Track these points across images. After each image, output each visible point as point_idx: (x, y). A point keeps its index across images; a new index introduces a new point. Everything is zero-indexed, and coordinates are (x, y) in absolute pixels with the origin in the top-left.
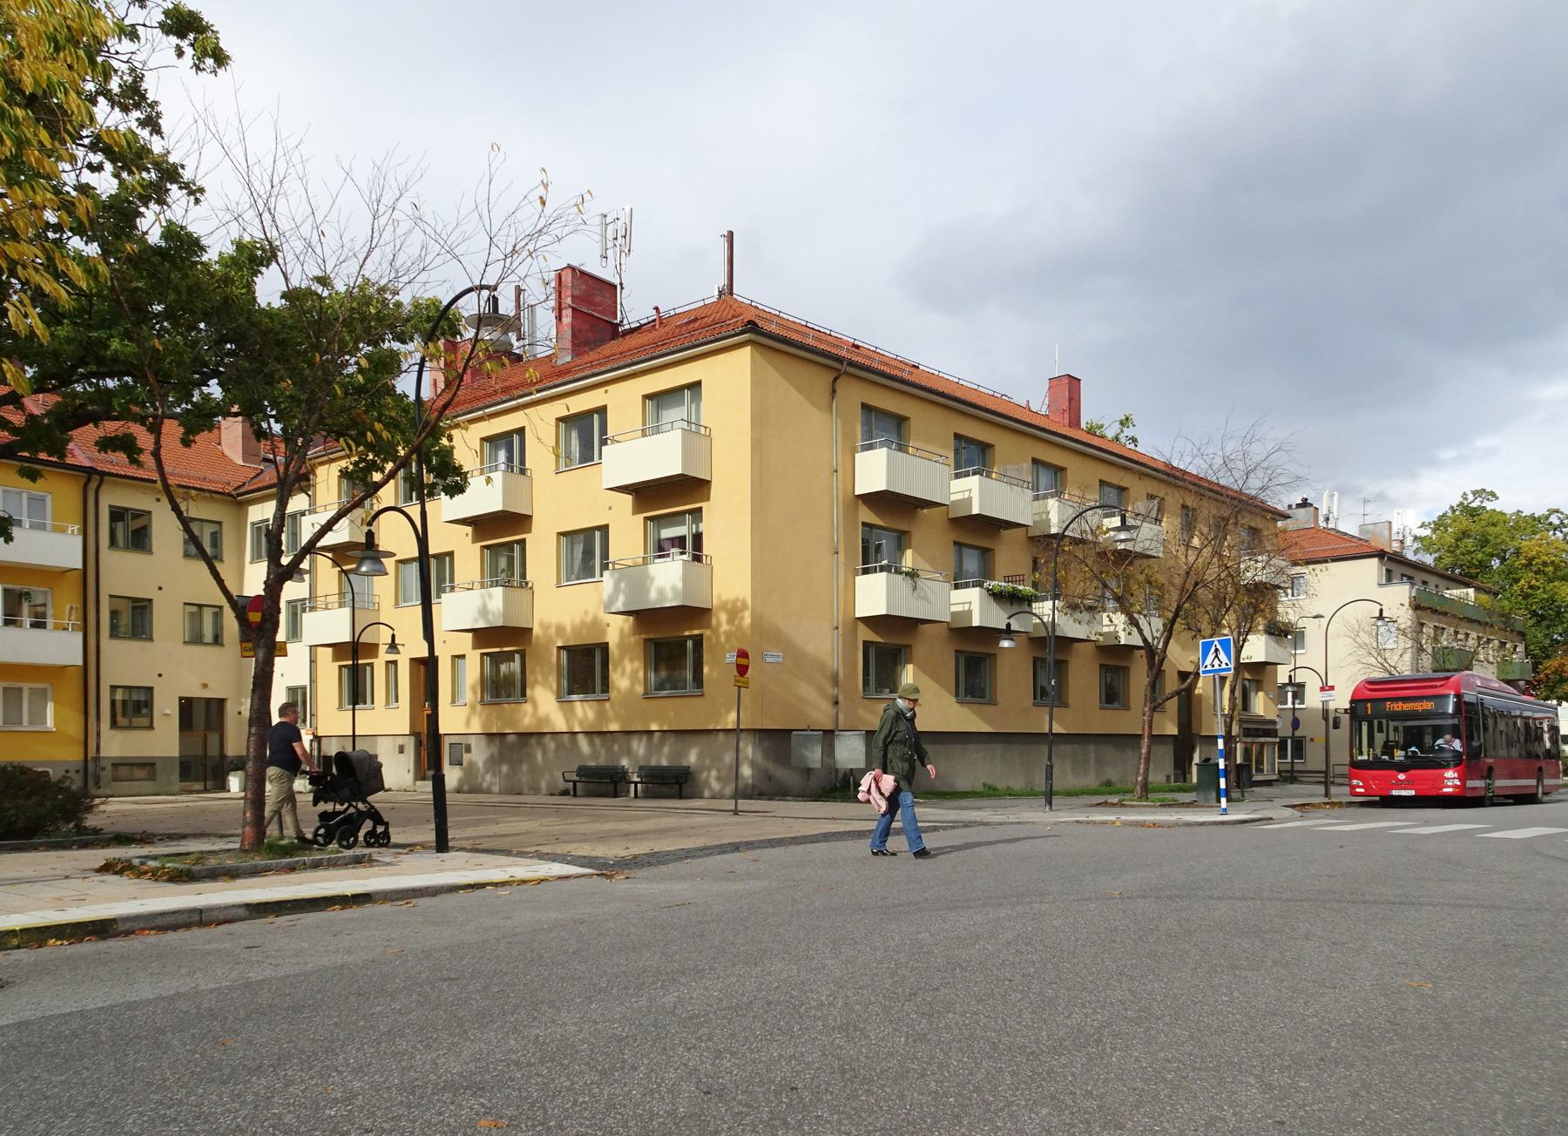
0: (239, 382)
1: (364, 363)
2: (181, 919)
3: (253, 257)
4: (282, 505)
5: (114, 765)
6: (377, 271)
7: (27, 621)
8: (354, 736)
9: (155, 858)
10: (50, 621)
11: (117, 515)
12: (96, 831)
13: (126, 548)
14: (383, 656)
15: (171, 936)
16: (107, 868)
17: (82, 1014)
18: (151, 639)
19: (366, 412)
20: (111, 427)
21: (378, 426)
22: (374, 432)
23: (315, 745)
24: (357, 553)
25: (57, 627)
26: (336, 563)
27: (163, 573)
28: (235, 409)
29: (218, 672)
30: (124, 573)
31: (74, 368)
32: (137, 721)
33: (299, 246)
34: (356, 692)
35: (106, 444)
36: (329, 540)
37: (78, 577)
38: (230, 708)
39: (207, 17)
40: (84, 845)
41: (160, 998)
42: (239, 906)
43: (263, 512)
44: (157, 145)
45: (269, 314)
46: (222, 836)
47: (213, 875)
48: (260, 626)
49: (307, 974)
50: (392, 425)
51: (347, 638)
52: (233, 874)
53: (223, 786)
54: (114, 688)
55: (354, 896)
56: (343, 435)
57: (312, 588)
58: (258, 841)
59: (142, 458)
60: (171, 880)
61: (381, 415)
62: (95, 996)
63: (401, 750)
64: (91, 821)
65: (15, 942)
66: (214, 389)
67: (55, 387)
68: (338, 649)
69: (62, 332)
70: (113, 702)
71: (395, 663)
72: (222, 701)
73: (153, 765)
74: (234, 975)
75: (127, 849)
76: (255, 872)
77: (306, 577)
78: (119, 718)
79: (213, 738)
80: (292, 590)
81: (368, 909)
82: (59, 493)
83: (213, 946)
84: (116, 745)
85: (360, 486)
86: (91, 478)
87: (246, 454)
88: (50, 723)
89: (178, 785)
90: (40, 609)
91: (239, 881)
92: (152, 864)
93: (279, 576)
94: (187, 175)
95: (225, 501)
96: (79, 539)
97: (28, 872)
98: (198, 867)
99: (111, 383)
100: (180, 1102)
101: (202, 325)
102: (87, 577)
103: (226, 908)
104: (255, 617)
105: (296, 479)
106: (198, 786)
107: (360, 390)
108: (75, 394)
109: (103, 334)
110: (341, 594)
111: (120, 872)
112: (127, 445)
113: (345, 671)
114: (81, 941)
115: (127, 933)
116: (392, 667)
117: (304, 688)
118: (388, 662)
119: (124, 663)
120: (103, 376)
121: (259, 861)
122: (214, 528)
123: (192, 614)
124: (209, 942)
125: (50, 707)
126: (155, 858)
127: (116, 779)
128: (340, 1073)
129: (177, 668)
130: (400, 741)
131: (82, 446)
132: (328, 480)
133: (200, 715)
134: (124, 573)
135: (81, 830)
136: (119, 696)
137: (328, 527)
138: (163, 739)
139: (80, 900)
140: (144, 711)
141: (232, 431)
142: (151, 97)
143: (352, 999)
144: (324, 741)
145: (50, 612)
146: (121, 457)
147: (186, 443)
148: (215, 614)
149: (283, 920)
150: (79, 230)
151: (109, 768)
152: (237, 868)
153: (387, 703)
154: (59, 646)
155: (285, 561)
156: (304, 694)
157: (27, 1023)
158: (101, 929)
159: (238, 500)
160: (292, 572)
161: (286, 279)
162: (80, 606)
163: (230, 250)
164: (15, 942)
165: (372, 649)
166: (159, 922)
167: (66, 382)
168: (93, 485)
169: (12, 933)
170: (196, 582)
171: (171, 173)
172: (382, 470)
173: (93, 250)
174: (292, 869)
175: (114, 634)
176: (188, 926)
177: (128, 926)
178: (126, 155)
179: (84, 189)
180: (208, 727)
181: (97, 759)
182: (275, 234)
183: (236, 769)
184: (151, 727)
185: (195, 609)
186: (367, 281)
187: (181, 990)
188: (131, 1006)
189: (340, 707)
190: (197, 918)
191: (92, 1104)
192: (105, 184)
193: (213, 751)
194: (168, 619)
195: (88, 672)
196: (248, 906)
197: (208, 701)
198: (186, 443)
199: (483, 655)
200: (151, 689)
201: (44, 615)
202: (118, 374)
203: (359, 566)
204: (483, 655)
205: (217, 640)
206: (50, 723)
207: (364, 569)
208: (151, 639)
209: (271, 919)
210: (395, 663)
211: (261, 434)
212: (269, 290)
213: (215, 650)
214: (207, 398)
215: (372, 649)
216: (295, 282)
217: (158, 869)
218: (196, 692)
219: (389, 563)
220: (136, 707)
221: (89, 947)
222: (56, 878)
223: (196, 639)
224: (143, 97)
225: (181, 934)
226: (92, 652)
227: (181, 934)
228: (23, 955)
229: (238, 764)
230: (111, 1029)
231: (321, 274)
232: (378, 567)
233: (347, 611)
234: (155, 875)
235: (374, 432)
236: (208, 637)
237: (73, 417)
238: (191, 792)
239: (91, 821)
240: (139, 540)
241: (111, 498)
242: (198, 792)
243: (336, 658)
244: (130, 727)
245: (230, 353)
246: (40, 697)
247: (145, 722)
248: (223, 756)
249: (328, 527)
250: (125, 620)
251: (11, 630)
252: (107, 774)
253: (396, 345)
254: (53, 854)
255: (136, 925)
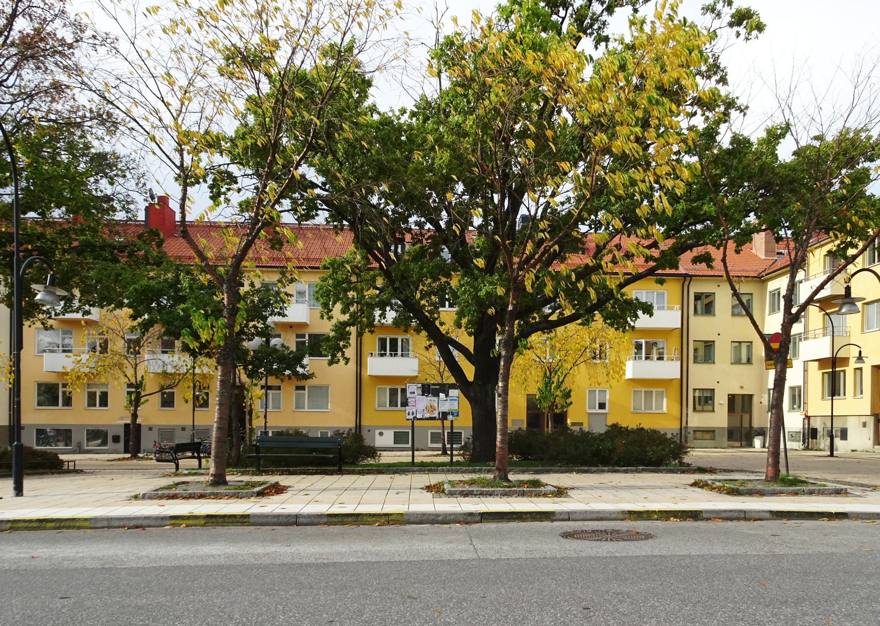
0: (765, 211)
1: (847, 181)
2: (735, 515)
3: (774, 136)
4: (793, 277)
5: (694, 431)
6: (853, 123)
7: (655, 356)
8: (832, 416)
9: (719, 481)
10: (665, 356)
11: (698, 297)
12: (688, 465)
13: (702, 314)
14: (853, 364)
15: (729, 523)
16: (695, 484)
17: (690, 556)
18: (714, 363)
19: (847, 210)
20: (697, 251)
21: (854, 219)
22: (852, 223)
23: (806, 421)
24: (840, 301)
25: (668, 359)
26: (821, 309)
27: (723, 326)
28: (763, 228)
29: (756, 380)
30: (702, 328)
31: (682, 222)
32: (707, 408)
33: (806, 121)
34: (834, 389)
35: (696, 260)
36: (822, 294)
37: (679, 331)
38: (755, 400)
39: (753, 9)
40: (683, 472)
41: (727, 555)
42: (766, 512)
43: (781, 284)
44: (723, 90)
45: (784, 166)
46: (753, 472)
47: (751, 493)
48: (779, 350)
49: (810, 555)
50: (866, 216)
51: (827, 354)
52: (761, 493)
53: (751, 445)
54: (695, 390)
55: (836, 513)
56: (832, 229)
57: (806, 327)
58: (775, 476)
59: (713, 264)
60: (728, 494)
61: (857, 211)
62: (696, 549)
63: (864, 425)
64: (686, 459)
65: (656, 517)
66: (752, 218)
67: (674, 235)
68: (822, 362)
69: (679, 207)
70: (694, 397)
71: (861, 369)
72: (751, 396)
73: (714, 431)
74: (766, 549)
75: (705, 476)
76: (774, 493)
77: (803, 320)
78: (697, 406)
79: (746, 417)
80: (797, 329)
81: (846, 522)
82: (672, 289)
83: (753, 532)
84: (696, 420)
85: (839, 259)
86: (687, 278)
87: (768, 252)
88: (665, 409)
89: (726, 443)
90: (661, 350)
91: (765, 498)
92: (718, 484)
93: (790, 319)
94: (739, 102)
95: (753, 281)
96: (680, 312)
97: (659, 483)
98: (742, 488)
99: (699, 227)
100: (744, 611)
101: (746, 184)
102: (683, 331)
103: (759, 512)
104: (775, 346)
105: (797, 264)
106: (737, 444)
107: (844, 198)
108: (682, 236)
109: (699, 203)
110: (824, 328)
111: (702, 487)
112: (706, 259)
113: (826, 376)
114: (685, 520)
115: (708, 519)
116: (858, 372)
117: (799, 387)
118: (855, 369)
119: (701, 376)
120: (695, 224)
121: (777, 487)
122: (749, 297)
123: (735, 347)
124: (751, 529)
125: (665, 400)
126: (719, 481)
127: (695, 439)
128: (836, 615)
129: (725, 378)
130: (864, 419)
131: (685, 262)
132: (817, 262)
133: (740, 404)
134: (702, 328)
135: (681, 464)
136: (697, 394)
137: (821, 287)
138: (719, 418)
139: (684, 499)
140: (710, 402)
141: (759, 240)
142: (722, 66)
143: (840, 574)
144: (812, 419)
145: (665, 352)
146: (704, 265)
147: (737, 252)
148: (748, 346)
149: (792, 522)
150: (689, 152)
151: (692, 433)
152: (764, 490)
153: (855, 395)
154: (669, 369)
155: (794, 310)
156: (800, 391)
157: (665, 556)
158: (695, 515)
159: (761, 279)
160: (796, 318)
161: (797, 143)
162: (679, 347)
163: (764, 135)
164: (656, 517)
165: (845, 361)
166: (723, 515)
167: (678, 231)
168: (687, 283)
169: (655, 512)
170: (743, 329)
171: (730, 104)
172: (856, 246)
173: (695, 159)
174: (796, 494)
175: (696, 361)
176: (738, 519)
177: (707, 515)
178: (705, 103)
179: (691, 129)
180: (743, 411)
181: (686, 428)
182: (791, 118)
183: (759, 435)
184: (713, 411)
185: (737, 344)
186: (848, 131)
187: (738, 552)
188: (713, 556)
189: (823, 398)
190: (743, 515)
191: (699, 602)
192: (699, 122)
193: (746, 424)
194: (723, 351)
195: (683, 381)
196: (771, 512)
197: (743, 396)
198: (737, 252)
199: (823, 373)
200: (713, 390)
201: (663, 354)
202: (702, 222)
203: (840, 310)
204: (823, 373)
205: (749, 361)
206: (665, 409)
207: (843, 310)
208: (714, 363)
209: (785, 521)
210: (861, 369)
211: (779, 239)
212: (785, 152)
213: (748, 366)
214: (748, 224)
215: (845, 361)
216: (803, 143)
217: (721, 487)
218: (738, 391)
219: (859, 304)
220: (706, 399)
221: (689, 524)
222: (672, 487)
223: (737, 361)
224: (719, 67)
225: (734, 523)
226: (684, 372)
227: (735, 523)
228: (659, 523)
229: (762, 432)
230: (705, 566)
231: (817, 133)
232: (853, 308)
233: (828, 339)
234: (720, 490)
235: (852, 223)
236: (744, 360)
237: (681, 248)
238: (733, 447)
239: (686, 459)
240: (708, 309)
241: (697, 288)
242: (737, 447)
243: (821, 367)
244: (703, 411)
245: (762, 195)
246: (660, 395)
247: (710, 408)
248: (751, 427)
249: (821, 287)
250: (701, 353)
251: (648, 361)
252: (691, 436)
253: (867, 165)
254: (669, 475)
255: (712, 516)
